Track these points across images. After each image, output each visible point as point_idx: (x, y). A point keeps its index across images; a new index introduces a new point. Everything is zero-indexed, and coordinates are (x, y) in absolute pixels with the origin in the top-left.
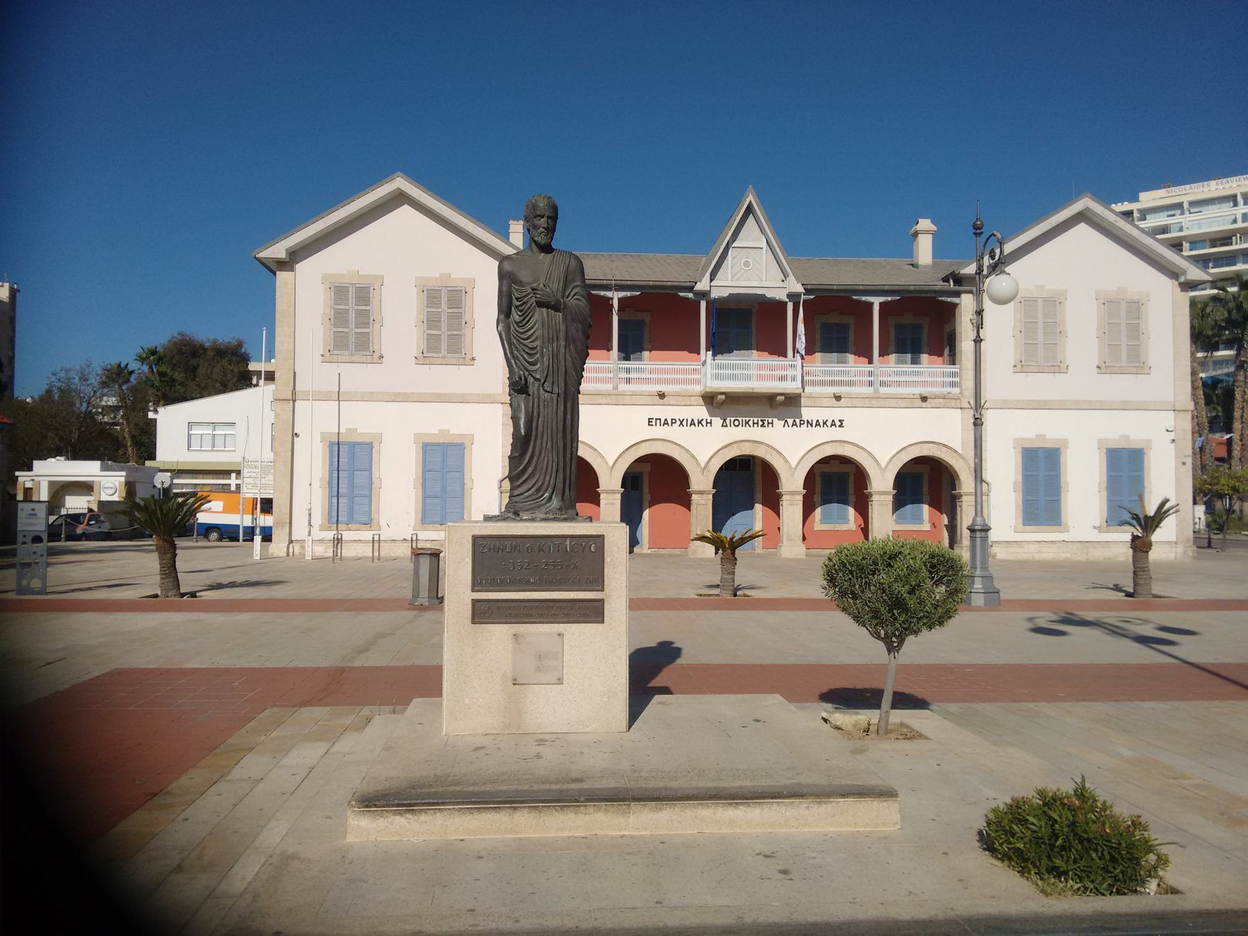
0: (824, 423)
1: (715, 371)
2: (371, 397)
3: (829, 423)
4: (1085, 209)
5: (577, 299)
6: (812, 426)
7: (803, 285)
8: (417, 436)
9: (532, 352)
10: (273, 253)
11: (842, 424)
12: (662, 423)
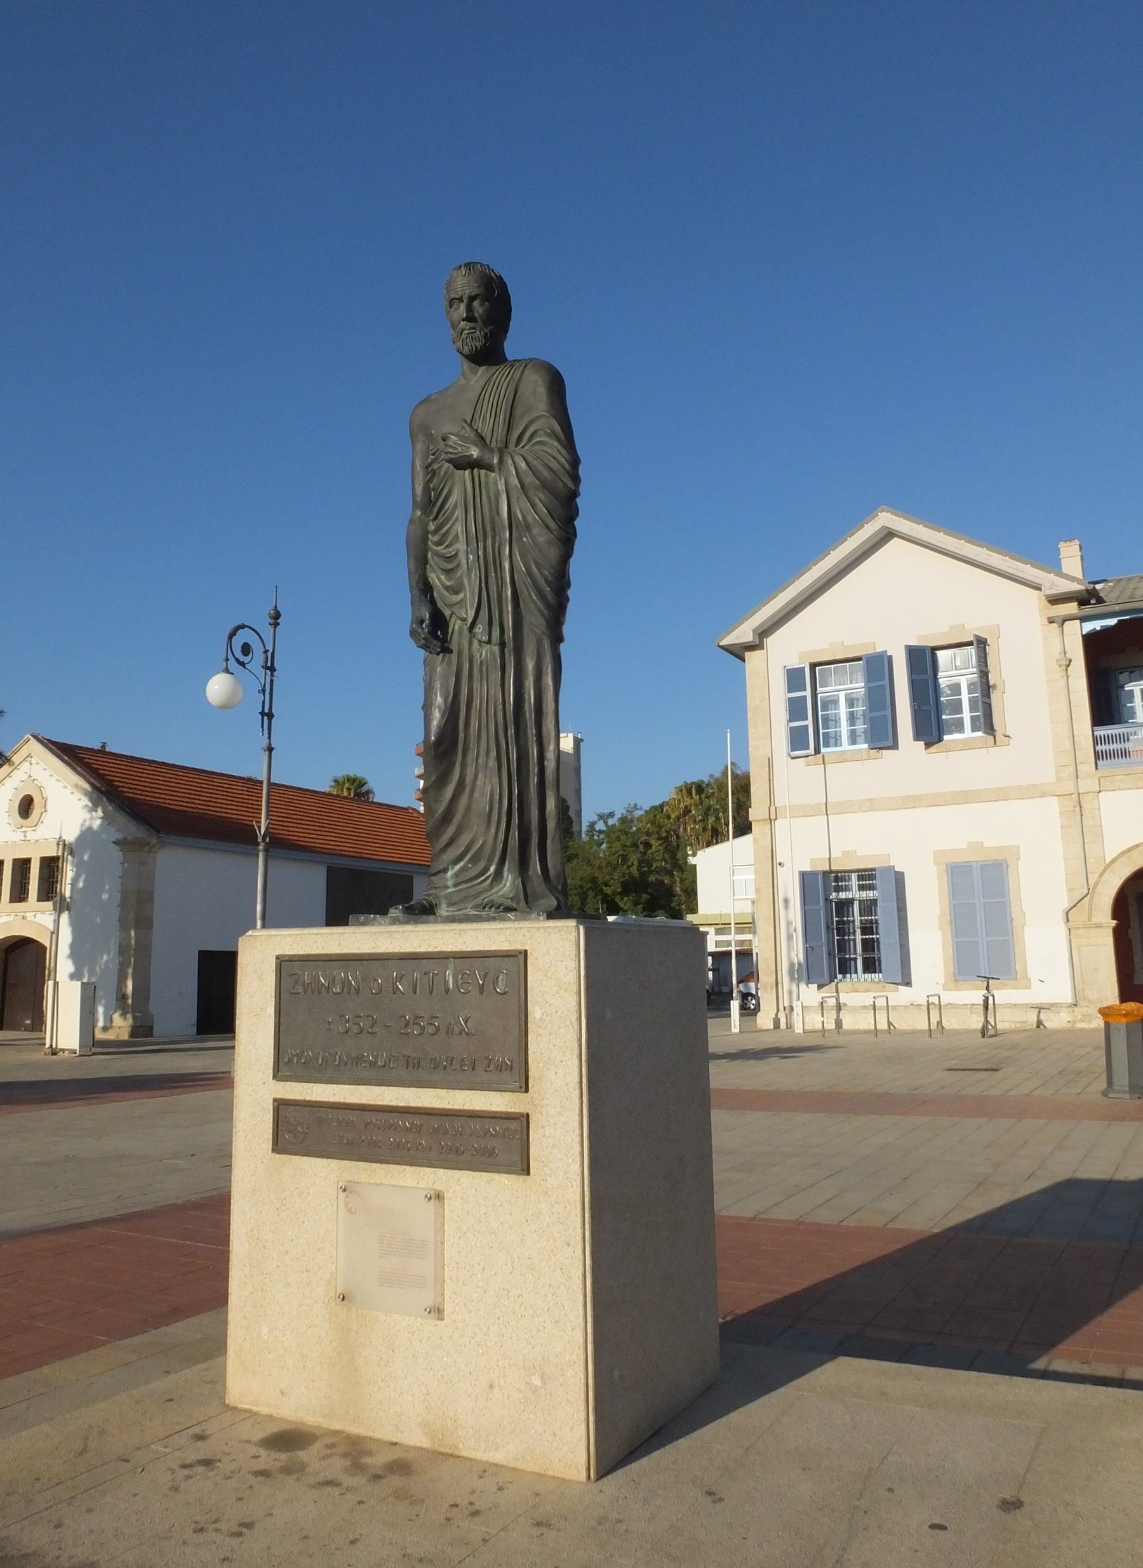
2: (871, 805)
5: (539, 443)
8: (938, 855)
9: (450, 566)
10: (738, 637)
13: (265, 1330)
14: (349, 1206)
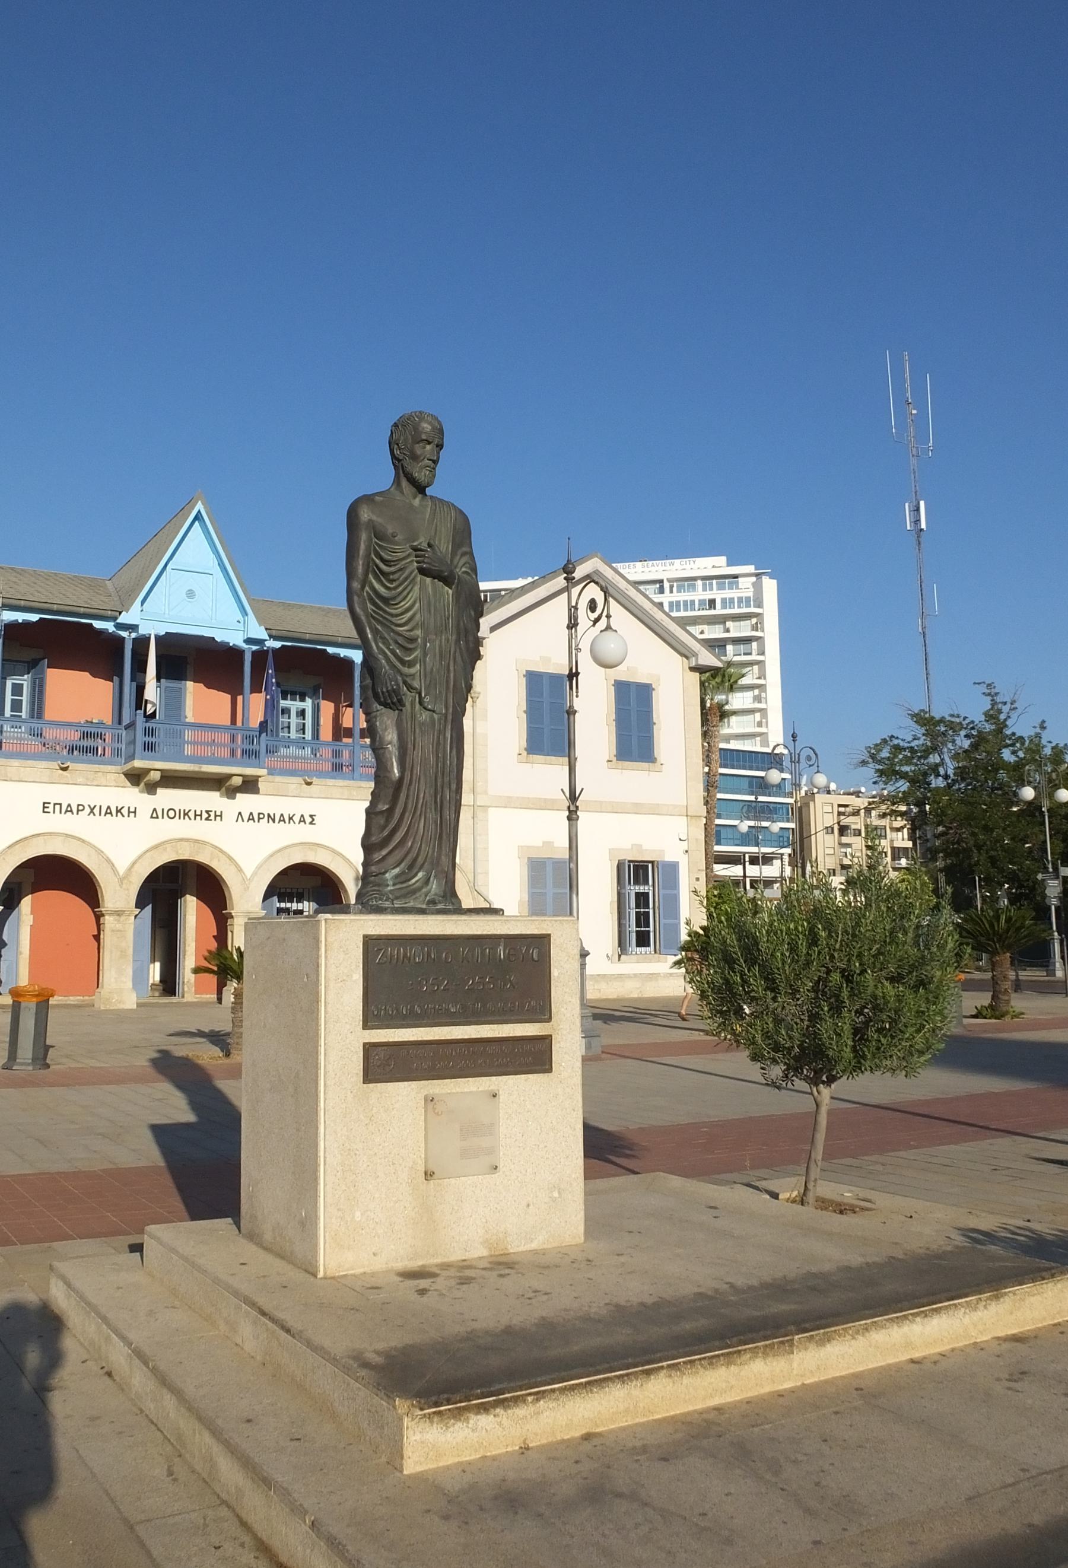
0: (291, 818)
1: (157, 740)
3: (296, 819)
4: (594, 572)
6: (274, 821)
7: (266, 629)
9: (411, 646)
11: (313, 820)
12: (63, 810)
13: (358, 1214)
14: (436, 1111)
